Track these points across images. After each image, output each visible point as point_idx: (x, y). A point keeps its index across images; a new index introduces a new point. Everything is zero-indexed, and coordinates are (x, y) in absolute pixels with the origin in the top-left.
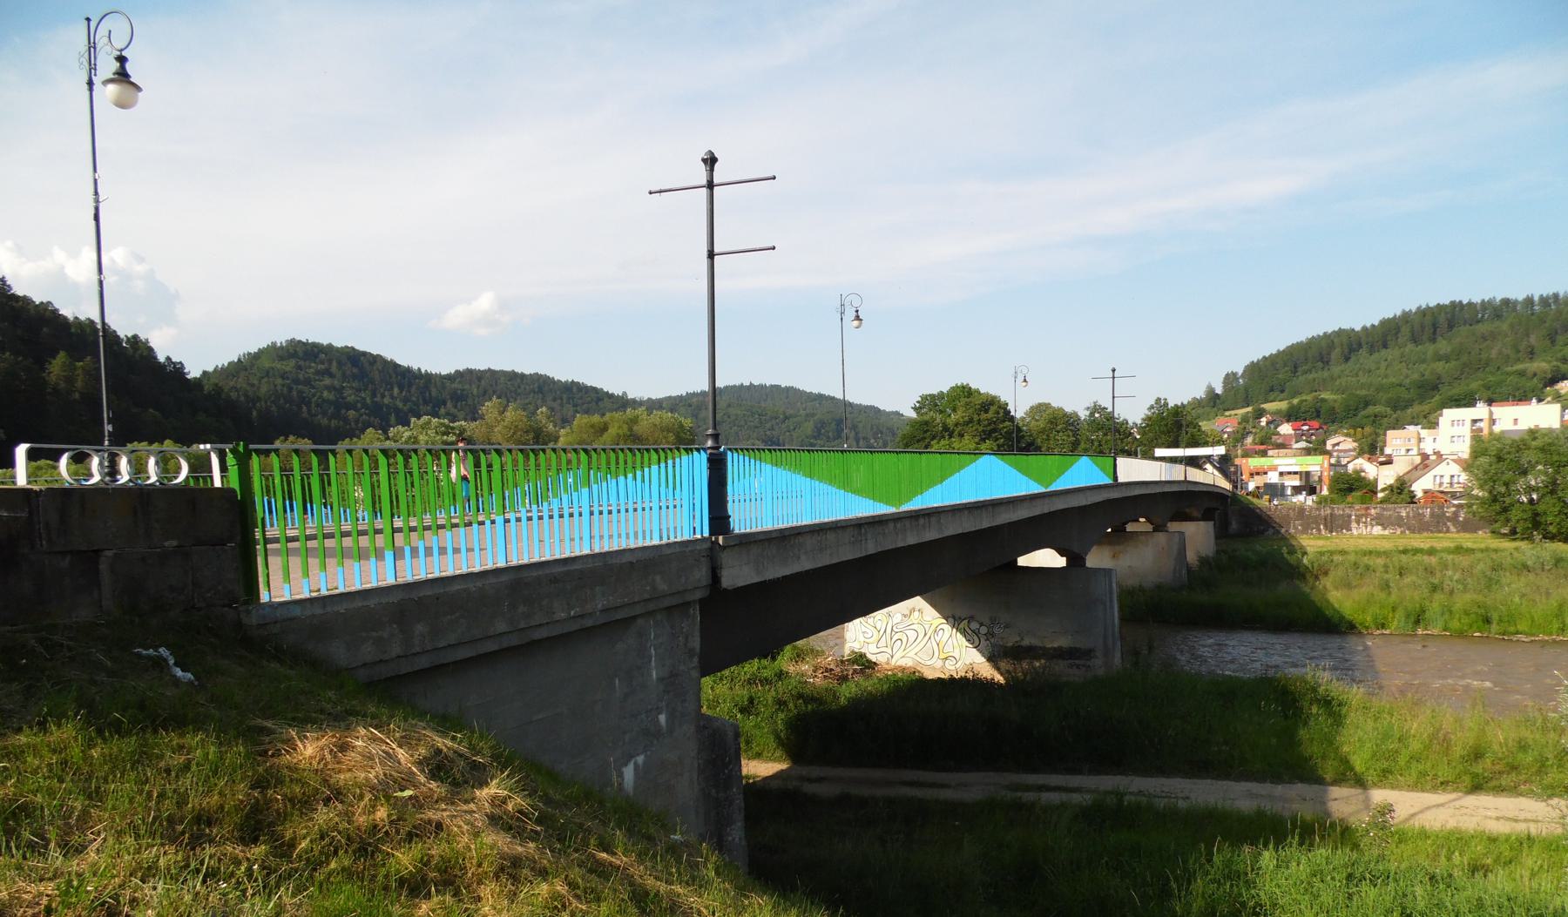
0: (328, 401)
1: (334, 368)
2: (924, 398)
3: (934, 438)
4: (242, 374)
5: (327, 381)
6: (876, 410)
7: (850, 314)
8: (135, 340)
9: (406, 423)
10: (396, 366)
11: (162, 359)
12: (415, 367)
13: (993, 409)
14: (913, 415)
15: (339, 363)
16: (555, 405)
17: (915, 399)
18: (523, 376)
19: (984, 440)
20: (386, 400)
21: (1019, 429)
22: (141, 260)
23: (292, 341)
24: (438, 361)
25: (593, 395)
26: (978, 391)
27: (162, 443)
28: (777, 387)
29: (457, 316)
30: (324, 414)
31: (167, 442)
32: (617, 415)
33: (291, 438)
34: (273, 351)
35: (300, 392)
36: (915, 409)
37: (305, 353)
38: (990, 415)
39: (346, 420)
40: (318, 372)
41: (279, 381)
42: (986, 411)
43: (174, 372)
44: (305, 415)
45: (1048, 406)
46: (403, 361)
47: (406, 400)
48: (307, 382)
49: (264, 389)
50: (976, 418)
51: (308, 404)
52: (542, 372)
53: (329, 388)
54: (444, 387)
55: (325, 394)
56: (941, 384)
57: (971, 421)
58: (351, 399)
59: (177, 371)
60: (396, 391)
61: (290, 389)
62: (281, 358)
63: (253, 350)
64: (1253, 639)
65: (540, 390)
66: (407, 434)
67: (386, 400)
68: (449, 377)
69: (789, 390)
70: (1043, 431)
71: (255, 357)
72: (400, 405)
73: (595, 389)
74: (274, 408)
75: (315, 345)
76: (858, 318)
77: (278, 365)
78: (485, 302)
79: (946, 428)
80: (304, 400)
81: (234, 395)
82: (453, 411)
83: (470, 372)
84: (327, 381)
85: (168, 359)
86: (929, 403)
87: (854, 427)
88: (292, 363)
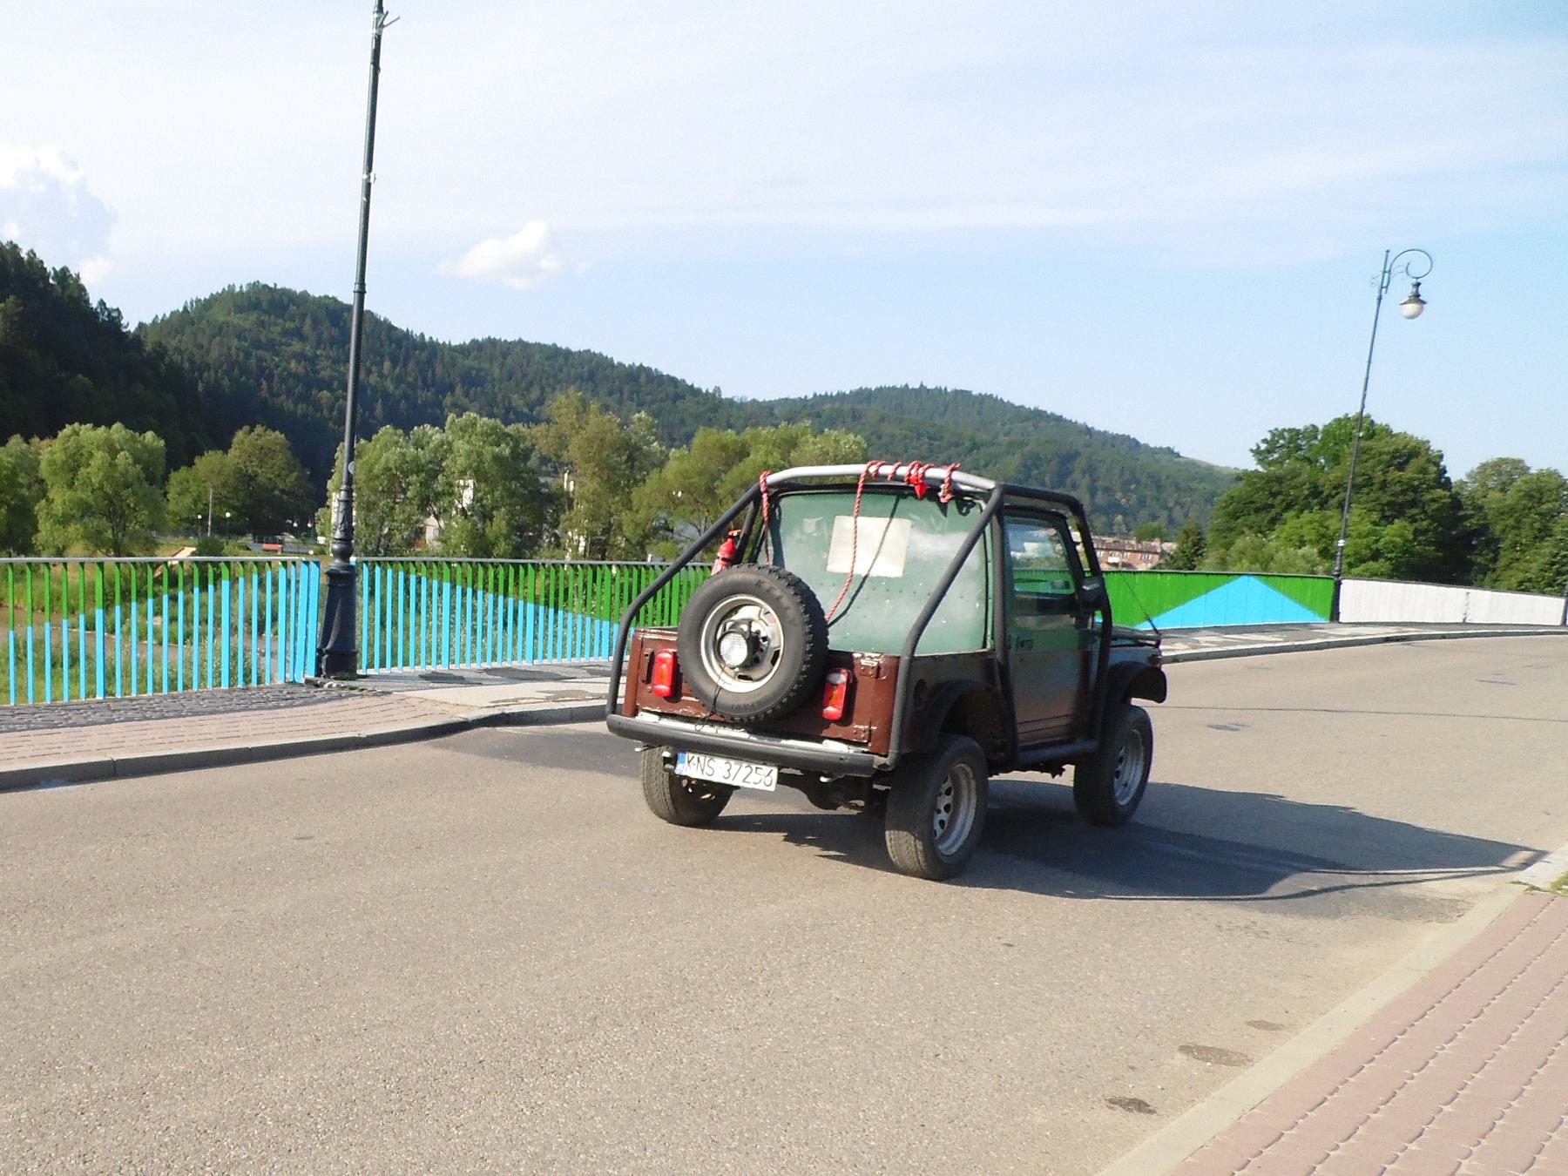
0: (296, 376)
1: (307, 328)
2: (1277, 434)
3: (1289, 507)
4: (188, 330)
5: (297, 346)
6: (1134, 444)
7: (1401, 288)
8: (63, 275)
9: (439, 422)
10: (391, 328)
11: (94, 304)
12: (417, 333)
13: (1415, 464)
14: (1252, 465)
15: (316, 322)
16: (611, 401)
17: (1258, 435)
18: (568, 353)
19: (1388, 520)
20: (373, 379)
21: (1456, 503)
22: (73, 165)
23: (256, 284)
24: (447, 326)
25: (670, 389)
26: (1386, 431)
27: (109, 425)
28: (964, 394)
29: (483, 258)
30: (289, 393)
31: (117, 426)
32: (764, 432)
33: (259, 429)
34: (232, 300)
35: (260, 360)
36: (1257, 452)
37: (272, 303)
38: (1409, 473)
39: (317, 405)
40: (285, 333)
41: (235, 342)
42: (1401, 467)
43: (105, 326)
44: (264, 394)
45: (1518, 466)
46: (400, 323)
47: (398, 381)
48: (271, 346)
49: (215, 353)
50: (1378, 476)
51: (270, 378)
52: (596, 349)
53: (300, 357)
54: (454, 365)
55: (293, 364)
56: (1317, 410)
57: (1369, 482)
58: (325, 374)
59: (114, 320)
60: (387, 364)
61: (248, 356)
62: (240, 310)
63: (204, 295)
64: (1257, 916)
65: (592, 376)
66: (437, 437)
67: (373, 379)
68: (463, 350)
69: (984, 399)
70: (1511, 511)
71: (207, 305)
72: (391, 387)
73: (673, 380)
74: (226, 382)
75: (286, 293)
76: (1416, 298)
77: (236, 319)
78: (530, 237)
79: (1316, 492)
80: (264, 373)
81: (177, 358)
82: (464, 401)
83: (492, 342)
84: (297, 346)
85: (102, 303)
86: (1285, 444)
87: (1091, 470)
88: (254, 316)
